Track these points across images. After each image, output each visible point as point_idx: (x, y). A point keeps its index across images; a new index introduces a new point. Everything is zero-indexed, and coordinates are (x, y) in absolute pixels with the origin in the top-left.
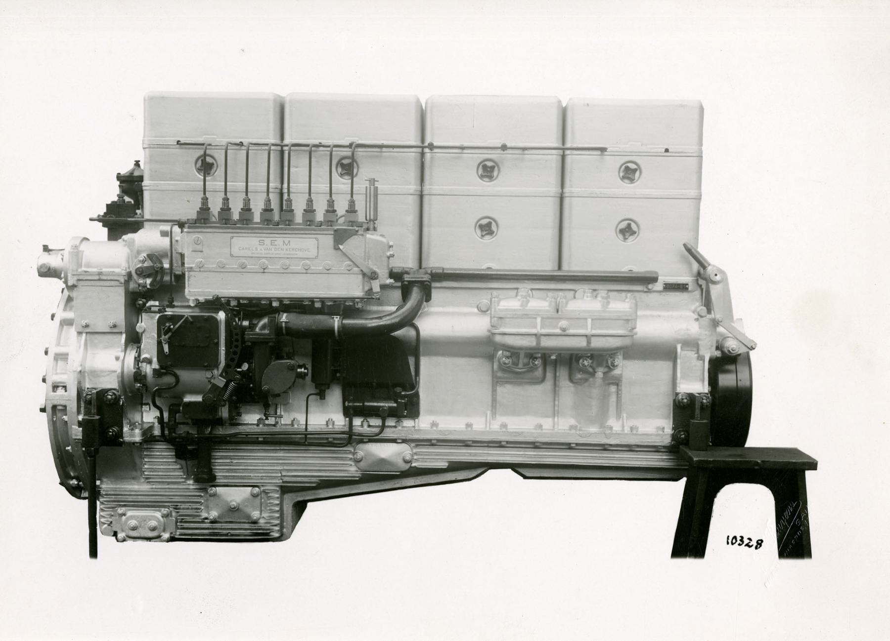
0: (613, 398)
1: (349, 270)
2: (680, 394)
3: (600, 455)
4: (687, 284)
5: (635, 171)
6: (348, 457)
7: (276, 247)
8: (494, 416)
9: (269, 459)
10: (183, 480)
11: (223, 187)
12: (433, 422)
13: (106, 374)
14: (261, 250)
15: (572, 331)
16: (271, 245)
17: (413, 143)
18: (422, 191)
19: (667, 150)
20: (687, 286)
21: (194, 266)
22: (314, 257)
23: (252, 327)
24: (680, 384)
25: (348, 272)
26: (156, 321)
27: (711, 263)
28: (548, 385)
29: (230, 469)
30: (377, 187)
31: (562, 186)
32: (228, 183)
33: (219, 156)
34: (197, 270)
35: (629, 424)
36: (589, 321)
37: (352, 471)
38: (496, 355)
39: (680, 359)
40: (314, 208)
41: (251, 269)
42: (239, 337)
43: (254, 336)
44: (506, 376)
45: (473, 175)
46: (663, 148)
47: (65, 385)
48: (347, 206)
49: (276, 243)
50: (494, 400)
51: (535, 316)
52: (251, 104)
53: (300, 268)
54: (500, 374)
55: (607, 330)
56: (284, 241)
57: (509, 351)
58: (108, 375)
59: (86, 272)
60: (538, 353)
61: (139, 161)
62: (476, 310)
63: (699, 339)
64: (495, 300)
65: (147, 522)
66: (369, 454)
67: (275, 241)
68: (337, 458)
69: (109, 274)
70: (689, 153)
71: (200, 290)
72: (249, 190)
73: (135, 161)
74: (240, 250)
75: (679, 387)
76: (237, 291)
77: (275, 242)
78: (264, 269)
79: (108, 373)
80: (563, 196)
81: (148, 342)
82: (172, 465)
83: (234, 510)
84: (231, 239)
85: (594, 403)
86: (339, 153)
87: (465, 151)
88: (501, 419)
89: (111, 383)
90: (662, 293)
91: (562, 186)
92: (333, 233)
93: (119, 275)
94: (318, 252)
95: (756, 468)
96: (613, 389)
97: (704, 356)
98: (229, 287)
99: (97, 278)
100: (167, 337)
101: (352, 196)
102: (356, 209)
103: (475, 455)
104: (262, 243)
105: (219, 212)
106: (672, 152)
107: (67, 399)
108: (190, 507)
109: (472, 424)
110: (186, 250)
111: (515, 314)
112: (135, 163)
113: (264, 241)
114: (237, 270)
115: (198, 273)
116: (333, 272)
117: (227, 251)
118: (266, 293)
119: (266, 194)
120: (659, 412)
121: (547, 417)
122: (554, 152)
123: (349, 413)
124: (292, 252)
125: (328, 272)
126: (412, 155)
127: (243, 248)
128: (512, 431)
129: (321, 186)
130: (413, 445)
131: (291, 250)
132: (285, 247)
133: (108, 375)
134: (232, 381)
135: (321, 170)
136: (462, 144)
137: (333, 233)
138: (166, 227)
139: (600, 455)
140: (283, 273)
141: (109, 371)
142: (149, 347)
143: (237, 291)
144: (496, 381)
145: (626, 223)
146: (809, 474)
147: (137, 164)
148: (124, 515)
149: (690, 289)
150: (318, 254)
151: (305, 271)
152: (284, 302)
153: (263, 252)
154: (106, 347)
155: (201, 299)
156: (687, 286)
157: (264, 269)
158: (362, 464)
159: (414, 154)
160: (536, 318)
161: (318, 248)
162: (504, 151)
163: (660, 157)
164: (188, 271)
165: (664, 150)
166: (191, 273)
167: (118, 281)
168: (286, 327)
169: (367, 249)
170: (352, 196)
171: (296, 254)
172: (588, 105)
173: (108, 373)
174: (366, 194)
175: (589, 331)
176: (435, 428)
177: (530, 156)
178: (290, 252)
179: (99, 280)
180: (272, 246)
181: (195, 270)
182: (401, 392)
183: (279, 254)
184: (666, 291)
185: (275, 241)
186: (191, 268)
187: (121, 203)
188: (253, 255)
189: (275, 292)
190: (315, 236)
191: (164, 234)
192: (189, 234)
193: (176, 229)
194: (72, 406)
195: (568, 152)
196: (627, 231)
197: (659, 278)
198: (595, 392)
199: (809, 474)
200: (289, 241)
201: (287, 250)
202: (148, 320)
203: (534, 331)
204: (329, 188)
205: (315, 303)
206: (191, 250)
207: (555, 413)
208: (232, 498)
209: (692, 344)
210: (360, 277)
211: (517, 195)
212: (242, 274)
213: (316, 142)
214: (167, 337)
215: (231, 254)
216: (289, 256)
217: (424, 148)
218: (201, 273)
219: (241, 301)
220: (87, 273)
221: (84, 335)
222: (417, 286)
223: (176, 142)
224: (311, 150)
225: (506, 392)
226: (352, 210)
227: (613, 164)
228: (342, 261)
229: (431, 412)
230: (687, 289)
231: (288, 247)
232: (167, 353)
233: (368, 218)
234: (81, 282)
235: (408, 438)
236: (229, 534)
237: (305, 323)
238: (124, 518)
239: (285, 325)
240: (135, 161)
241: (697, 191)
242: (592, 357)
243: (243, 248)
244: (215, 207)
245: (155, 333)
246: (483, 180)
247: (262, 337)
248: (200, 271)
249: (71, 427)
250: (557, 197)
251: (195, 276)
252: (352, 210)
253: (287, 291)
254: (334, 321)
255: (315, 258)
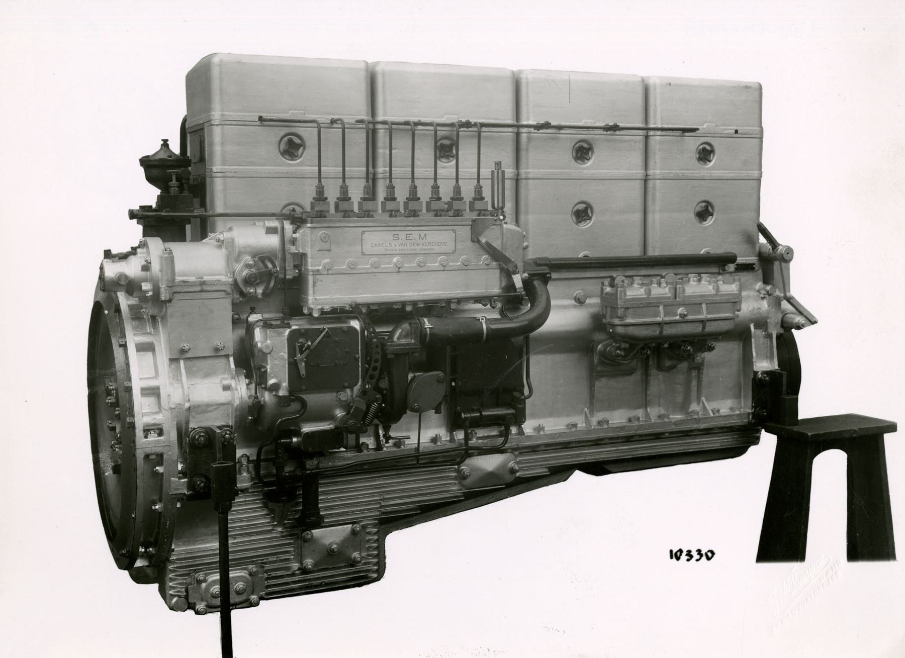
0: (694, 383)
1: (487, 265)
2: (760, 373)
3: (684, 442)
4: (754, 264)
5: (299, 146)
6: (451, 476)
7: (411, 241)
8: (592, 413)
9: (334, 494)
10: (270, 528)
11: (454, 174)
12: (539, 425)
13: (212, 408)
14: (395, 245)
15: (690, 317)
16: (407, 239)
17: (510, 122)
18: (518, 175)
19: (736, 132)
20: (754, 266)
21: (320, 268)
22: (452, 252)
23: (392, 334)
24: (755, 362)
25: (487, 267)
26: (286, 338)
27: (780, 243)
28: (638, 376)
29: (327, 507)
30: (504, 171)
31: (646, 167)
32: (346, 169)
33: (308, 134)
34: (325, 273)
35: (710, 406)
36: (704, 306)
37: (455, 489)
38: (597, 349)
39: (754, 338)
40: (349, 196)
41: (385, 268)
42: (379, 349)
43: (398, 347)
44: (606, 369)
45: (567, 156)
46: (733, 129)
47: (160, 427)
48: (452, 193)
49: (411, 237)
50: (592, 396)
51: (658, 305)
52: (755, 83)
53: (437, 264)
54: (599, 368)
55: (719, 314)
56: (420, 235)
57: (627, 342)
58: (216, 409)
59: (184, 282)
60: (653, 342)
61: (167, 140)
62: (573, 302)
63: (767, 317)
64: (621, 290)
65: (234, 585)
66: (475, 469)
67: (411, 234)
68: (442, 478)
69: (213, 283)
70: (754, 134)
71: (327, 297)
72: (460, 177)
73: (162, 140)
74: (372, 247)
75: (756, 366)
76: (369, 295)
77: (411, 236)
78: (399, 268)
79: (216, 407)
80: (376, 177)
81: (275, 364)
82: (259, 511)
83: (330, 553)
84: (362, 234)
85: (680, 388)
86: (442, 132)
87: (562, 131)
88: (600, 416)
89: (216, 421)
90: (733, 274)
91: (646, 167)
92: (471, 223)
93: (225, 283)
94: (455, 246)
95: (855, 435)
96: (694, 373)
97: (772, 334)
98: (360, 292)
99: (199, 289)
100: (304, 355)
101: (320, 181)
102: (418, 196)
103: (578, 456)
104: (396, 237)
105: (311, 202)
106: (742, 134)
107: (164, 445)
108: (278, 559)
109: (577, 424)
110: (309, 250)
111: (641, 303)
112: (162, 142)
113: (398, 235)
114: (370, 271)
115: (325, 276)
116: (472, 267)
117: (359, 248)
118: (401, 296)
119: (317, 180)
120: (732, 392)
121: (639, 408)
122: (510, 129)
123: (454, 424)
124: (429, 247)
125: (466, 268)
126: (509, 133)
127: (376, 244)
128: (615, 426)
129: (424, 168)
130: (516, 453)
131: (428, 244)
132: (421, 241)
133: (216, 409)
134: (373, 402)
135: (425, 154)
136: (559, 123)
137: (471, 223)
138: (274, 223)
139: (684, 442)
140: (419, 272)
141: (216, 405)
142: (634, 363)
143: (369, 295)
144: (594, 375)
145: (583, 206)
146: (887, 437)
147: (165, 144)
148: (205, 581)
149: (756, 268)
150: (456, 249)
151: (442, 268)
152: (419, 306)
153: (398, 247)
154: (207, 375)
155: (327, 308)
156: (754, 266)
157: (399, 268)
158: (468, 482)
159: (511, 134)
160: (659, 306)
161: (455, 241)
162: (538, 130)
163: (727, 138)
164: (313, 275)
165: (734, 131)
166: (318, 277)
167: (225, 291)
168: (430, 334)
169: (504, 241)
170: (320, 181)
171: (433, 249)
172: (670, 84)
173: (216, 407)
174: (492, 179)
175: (703, 316)
176: (542, 433)
177: (621, 136)
178: (426, 247)
179: (202, 291)
180: (406, 241)
181: (322, 273)
182: (520, 397)
183: (415, 250)
184: (738, 272)
185: (411, 234)
186: (318, 271)
187: (176, 194)
188: (387, 252)
189: (410, 294)
190: (453, 227)
191: (271, 231)
192: (314, 230)
193: (288, 227)
194: (172, 453)
195: (651, 133)
196: (704, 214)
197: (738, 259)
198: (681, 378)
199: (887, 437)
200: (426, 235)
201: (423, 244)
202: (276, 336)
203: (659, 319)
204: (433, 173)
205: (452, 304)
206: (318, 249)
207: (645, 404)
208: (331, 541)
209: (761, 324)
210: (498, 271)
211: (734, 178)
212: (375, 276)
213: (416, 119)
214: (304, 355)
215: (362, 252)
216: (427, 252)
217: (517, 126)
218: (330, 276)
219: (372, 307)
220: (186, 284)
221: (182, 362)
222: (536, 279)
223: (257, 118)
224: (411, 128)
225: (602, 384)
226: (479, 197)
227: (692, 144)
228: (480, 255)
229: (534, 416)
230: (754, 268)
231: (424, 241)
232: (303, 375)
233: (496, 206)
234: (176, 295)
235: (520, 446)
236: (323, 583)
237: (451, 327)
238: (204, 585)
239: (430, 331)
240: (162, 140)
241: (759, 172)
242: (691, 343)
243: (376, 244)
244: (332, 193)
245: (285, 352)
246: (577, 162)
247: (407, 347)
248: (328, 274)
249: (170, 481)
250: (514, 179)
251: (322, 281)
252: (479, 197)
253: (424, 292)
254: (481, 322)
255: (453, 253)
